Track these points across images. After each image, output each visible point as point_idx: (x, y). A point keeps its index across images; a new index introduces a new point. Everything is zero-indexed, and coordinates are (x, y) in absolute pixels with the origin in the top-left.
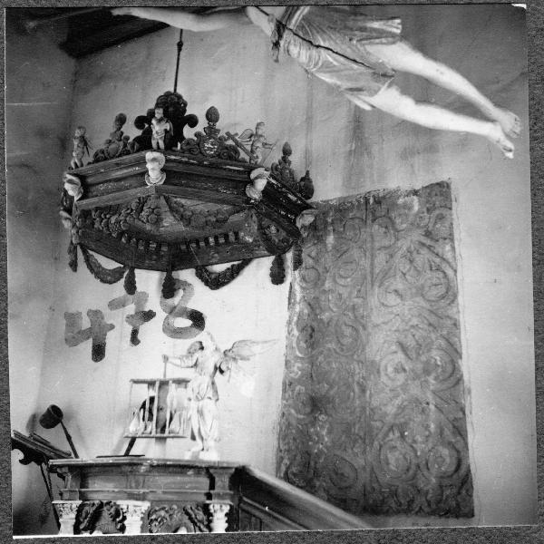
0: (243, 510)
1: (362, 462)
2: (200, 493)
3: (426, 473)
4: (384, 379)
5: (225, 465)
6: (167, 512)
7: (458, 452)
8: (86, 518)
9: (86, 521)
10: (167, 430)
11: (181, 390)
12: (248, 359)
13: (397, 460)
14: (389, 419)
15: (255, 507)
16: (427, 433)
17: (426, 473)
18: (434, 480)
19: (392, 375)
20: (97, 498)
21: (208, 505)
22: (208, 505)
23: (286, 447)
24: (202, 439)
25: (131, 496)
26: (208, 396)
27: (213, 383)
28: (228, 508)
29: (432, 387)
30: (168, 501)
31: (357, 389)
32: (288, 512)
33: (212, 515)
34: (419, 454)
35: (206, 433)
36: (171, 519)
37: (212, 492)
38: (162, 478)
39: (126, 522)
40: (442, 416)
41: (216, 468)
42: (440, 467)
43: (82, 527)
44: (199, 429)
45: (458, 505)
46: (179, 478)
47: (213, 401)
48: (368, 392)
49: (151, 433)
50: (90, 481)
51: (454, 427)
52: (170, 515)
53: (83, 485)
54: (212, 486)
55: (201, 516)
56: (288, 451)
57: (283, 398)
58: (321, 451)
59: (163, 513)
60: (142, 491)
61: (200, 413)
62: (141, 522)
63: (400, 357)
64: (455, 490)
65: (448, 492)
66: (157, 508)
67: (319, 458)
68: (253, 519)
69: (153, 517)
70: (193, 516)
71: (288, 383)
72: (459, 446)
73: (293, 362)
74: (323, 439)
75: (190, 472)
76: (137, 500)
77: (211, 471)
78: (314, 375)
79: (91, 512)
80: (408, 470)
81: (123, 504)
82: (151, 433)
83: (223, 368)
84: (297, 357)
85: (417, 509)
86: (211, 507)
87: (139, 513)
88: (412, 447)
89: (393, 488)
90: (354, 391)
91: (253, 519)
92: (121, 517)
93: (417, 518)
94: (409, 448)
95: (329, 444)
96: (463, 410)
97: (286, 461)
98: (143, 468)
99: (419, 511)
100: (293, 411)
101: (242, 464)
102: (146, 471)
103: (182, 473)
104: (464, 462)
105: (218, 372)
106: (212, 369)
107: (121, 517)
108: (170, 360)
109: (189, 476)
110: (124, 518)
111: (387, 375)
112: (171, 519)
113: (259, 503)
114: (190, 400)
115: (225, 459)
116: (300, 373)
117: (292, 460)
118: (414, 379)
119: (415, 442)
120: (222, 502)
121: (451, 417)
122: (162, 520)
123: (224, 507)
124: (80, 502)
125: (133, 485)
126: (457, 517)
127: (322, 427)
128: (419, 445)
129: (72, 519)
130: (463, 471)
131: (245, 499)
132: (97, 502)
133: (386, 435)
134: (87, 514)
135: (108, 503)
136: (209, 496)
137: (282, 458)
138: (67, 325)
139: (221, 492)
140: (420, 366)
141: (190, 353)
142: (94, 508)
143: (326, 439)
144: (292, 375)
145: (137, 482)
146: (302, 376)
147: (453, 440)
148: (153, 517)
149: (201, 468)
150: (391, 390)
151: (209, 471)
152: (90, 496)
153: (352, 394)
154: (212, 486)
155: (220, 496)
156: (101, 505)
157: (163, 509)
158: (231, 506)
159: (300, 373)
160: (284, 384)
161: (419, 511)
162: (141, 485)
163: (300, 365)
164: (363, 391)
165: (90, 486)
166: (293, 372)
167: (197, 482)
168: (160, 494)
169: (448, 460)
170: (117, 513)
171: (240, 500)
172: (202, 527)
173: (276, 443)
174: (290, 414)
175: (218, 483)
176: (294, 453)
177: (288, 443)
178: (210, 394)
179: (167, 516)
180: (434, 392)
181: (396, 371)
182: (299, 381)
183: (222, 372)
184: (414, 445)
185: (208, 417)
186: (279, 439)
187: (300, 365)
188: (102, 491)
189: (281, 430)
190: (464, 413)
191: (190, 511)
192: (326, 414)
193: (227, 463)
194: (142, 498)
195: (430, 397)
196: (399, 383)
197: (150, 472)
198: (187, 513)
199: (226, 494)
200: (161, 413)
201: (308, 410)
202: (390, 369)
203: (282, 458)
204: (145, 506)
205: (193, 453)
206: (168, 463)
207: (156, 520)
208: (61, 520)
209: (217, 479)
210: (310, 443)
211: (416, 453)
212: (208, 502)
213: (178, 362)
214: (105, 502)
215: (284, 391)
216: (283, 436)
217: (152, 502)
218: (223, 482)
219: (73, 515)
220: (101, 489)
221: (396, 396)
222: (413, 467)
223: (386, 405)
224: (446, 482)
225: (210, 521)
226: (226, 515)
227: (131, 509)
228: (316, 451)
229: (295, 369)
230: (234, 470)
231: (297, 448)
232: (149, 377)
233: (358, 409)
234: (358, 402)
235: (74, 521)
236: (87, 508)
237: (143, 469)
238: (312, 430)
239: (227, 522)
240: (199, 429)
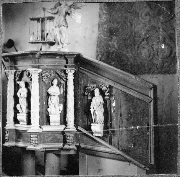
0: (80, 72)
1: (130, 54)
2: (63, 66)
3: (157, 57)
4: (140, 19)
5: (71, 54)
6: (49, 73)
7: (171, 48)
8: (17, 76)
9: (18, 78)
10: (46, 39)
11: (51, 23)
12: (80, 9)
13: (145, 53)
14: (143, 36)
15: (85, 71)
16: (158, 41)
17: (157, 57)
18: (160, 59)
19: (144, 17)
20: (21, 69)
21: (65, 70)
22: (65, 70)
23: (100, 50)
24: (62, 44)
25: (33, 67)
26: (63, 25)
27: (65, 20)
28: (74, 71)
29: (161, 21)
30: (47, 69)
31: (129, 25)
32: (102, 73)
33: (67, 74)
34: (154, 49)
35: (63, 41)
36: (51, 76)
37: (67, 65)
38: (46, 60)
39: (32, 77)
40: (165, 33)
41: (68, 55)
42: (163, 54)
43: (16, 80)
44: (60, 40)
45: (170, 69)
46: (53, 60)
47: (66, 27)
48: (134, 25)
49: (39, 41)
50: (18, 62)
51: (170, 37)
52: (50, 74)
53: (16, 63)
54: (67, 63)
55: (63, 74)
56: (101, 52)
57: (99, 31)
58: (114, 51)
59: (47, 73)
60: (37, 65)
61: (60, 32)
62: (38, 77)
63: (148, 9)
64: (169, 63)
65: (166, 64)
66: (45, 72)
67: (113, 54)
68: (84, 75)
69: (43, 75)
70: (60, 75)
71: (100, 24)
72: (172, 45)
73: (102, 15)
74: (115, 46)
75: (58, 57)
76: (35, 68)
77: (66, 56)
78: (111, 20)
79: (19, 74)
80: (149, 56)
81: (31, 70)
82: (39, 41)
83: (69, 12)
84: (104, 13)
85: (153, 72)
86: (67, 71)
87: (37, 73)
88: (152, 47)
89: (143, 64)
90: (127, 25)
91: (84, 75)
92: (31, 76)
93: (152, 75)
94: (150, 47)
95: (117, 48)
96: (174, 30)
97: (100, 56)
98: (37, 55)
99: (153, 72)
100: (103, 36)
101: (78, 53)
102: (39, 57)
103: (55, 58)
104: (173, 52)
105: (67, 15)
106: (64, 13)
107: (31, 76)
108: (46, 10)
109: (58, 59)
110: (32, 75)
111: (142, 17)
112: (51, 76)
113: (88, 70)
114: (56, 27)
115: (72, 51)
116: (105, 19)
117: (102, 55)
118: (153, 18)
119: (153, 45)
120: (71, 68)
121: (169, 33)
122: (47, 76)
123: (72, 71)
124: (15, 71)
125: (34, 62)
126: (169, 74)
127: (114, 42)
128: (154, 46)
129: (13, 77)
130: (173, 54)
131: (80, 67)
132: (21, 70)
133: (141, 43)
134: (18, 75)
135: (25, 70)
136: (66, 67)
137: (98, 55)
138: (157, 107)
139: (71, 65)
140: (156, 12)
141: (55, 8)
142: (20, 73)
143: (116, 46)
144: (102, 21)
145: (35, 61)
146: (106, 21)
147: (169, 43)
148: (43, 75)
149: (62, 55)
150: (144, 24)
151: (64, 56)
152: (18, 68)
153: (127, 27)
154: (67, 63)
155: (70, 67)
156: (23, 71)
157: (47, 72)
158: (75, 70)
159: (105, 19)
160: (99, 24)
161: (153, 72)
162: (37, 62)
163: (105, 16)
164: (132, 25)
165: (18, 64)
166: (102, 19)
167: (61, 61)
168: (45, 66)
169: (167, 51)
170: (29, 74)
171: (79, 68)
172: (64, 79)
173: (96, 49)
174: (101, 37)
175: (69, 61)
176: (103, 53)
177: (100, 49)
178: (64, 24)
179: (49, 75)
180: (162, 23)
181: (146, 15)
182: (105, 23)
183: (69, 14)
184: (153, 46)
185: (64, 34)
186: (97, 48)
187: (105, 16)
188: (23, 66)
189: (98, 44)
190: (175, 31)
191: (58, 73)
192: (116, 36)
193: (72, 53)
194: (38, 67)
195: (160, 25)
196: (147, 20)
197: (40, 57)
198: (58, 74)
199: (73, 66)
200: (43, 33)
201: (108, 35)
202: (143, 15)
203: (98, 55)
204: (40, 71)
205: (58, 49)
206: (47, 53)
207: (45, 76)
208: (8, 78)
209: (69, 60)
210: (110, 48)
211: (153, 49)
212: (65, 69)
213: (50, 11)
214: (24, 70)
215: (99, 27)
216: (98, 46)
217: (43, 69)
218: (71, 61)
219: (13, 76)
220: (22, 65)
221: (146, 26)
222: (152, 55)
223: (141, 30)
224: (166, 60)
225: (67, 76)
226: (73, 74)
227: (33, 72)
228: (112, 51)
229: (103, 18)
230: (75, 56)
231: (104, 50)
232: (37, 17)
233: (129, 33)
234: (129, 30)
235: (14, 78)
236: (17, 73)
237: (37, 56)
238: (110, 43)
239: (73, 76)
240: (60, 40)
